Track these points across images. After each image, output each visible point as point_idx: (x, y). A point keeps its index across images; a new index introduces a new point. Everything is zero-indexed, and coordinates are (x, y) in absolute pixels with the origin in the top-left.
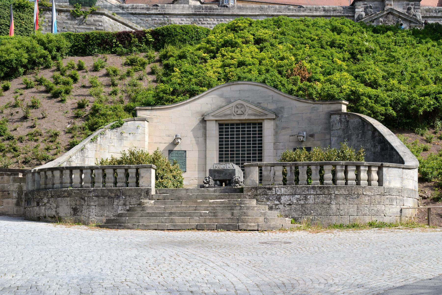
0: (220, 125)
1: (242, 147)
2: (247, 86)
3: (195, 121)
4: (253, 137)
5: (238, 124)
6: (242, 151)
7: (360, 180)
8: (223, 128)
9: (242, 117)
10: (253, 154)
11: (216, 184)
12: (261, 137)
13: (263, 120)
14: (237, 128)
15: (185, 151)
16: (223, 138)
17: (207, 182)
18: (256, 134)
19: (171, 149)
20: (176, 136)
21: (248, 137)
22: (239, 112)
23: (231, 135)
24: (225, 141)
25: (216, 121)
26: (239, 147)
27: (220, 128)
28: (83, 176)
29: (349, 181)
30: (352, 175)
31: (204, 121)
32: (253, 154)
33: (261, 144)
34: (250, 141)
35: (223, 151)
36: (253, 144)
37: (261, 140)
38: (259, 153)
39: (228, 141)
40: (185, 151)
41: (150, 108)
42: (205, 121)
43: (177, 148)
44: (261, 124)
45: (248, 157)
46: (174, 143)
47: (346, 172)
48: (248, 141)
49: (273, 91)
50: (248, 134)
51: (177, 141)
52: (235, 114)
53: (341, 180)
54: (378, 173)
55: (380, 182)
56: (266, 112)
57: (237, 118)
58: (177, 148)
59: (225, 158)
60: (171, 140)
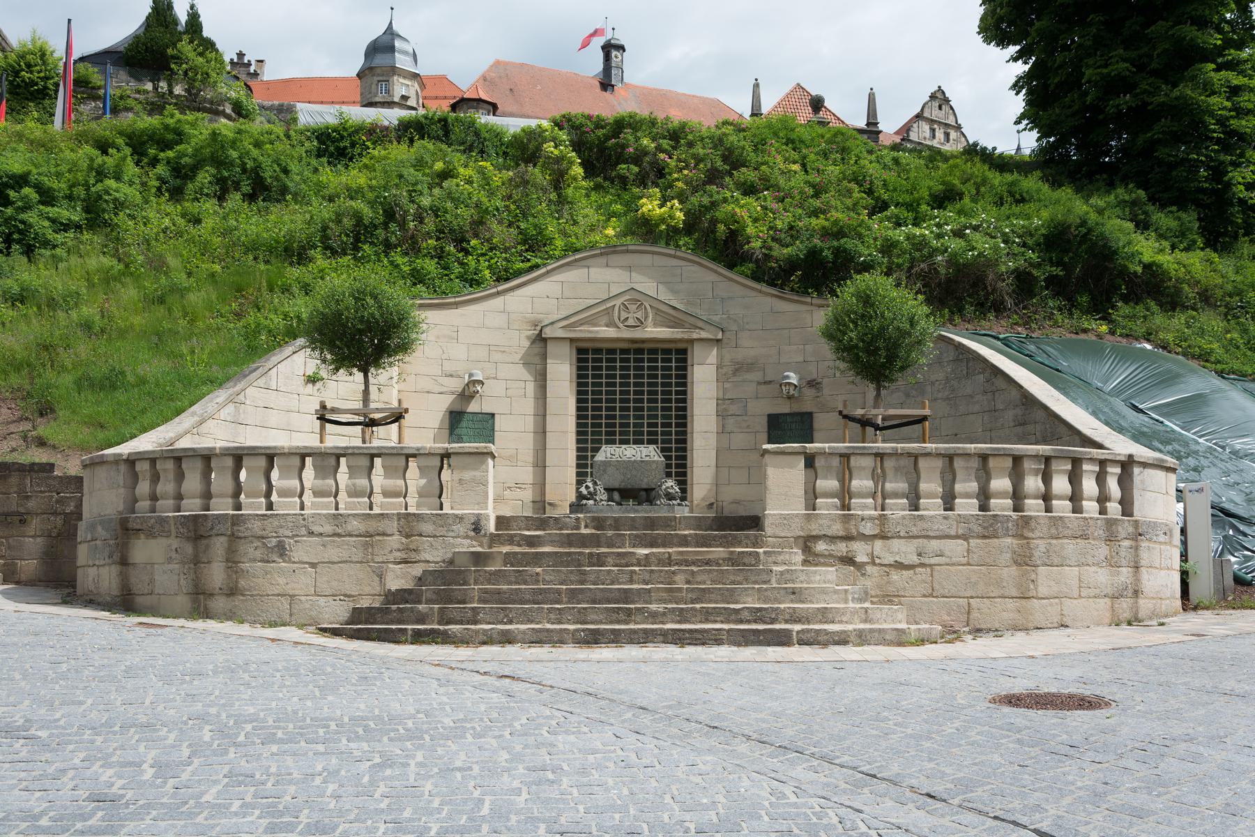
0: (580, 351)
1: (636, 409)
2: (649, 257)
3: (520, 341)
4: (663, 385)
5: (623, 351)
6: (636, 417)
7: (1082, 499)
8: (586, 360)
9: (637, 334)
10: (663, 425)
11: (610, 499)
12: (685, 385)
13: (692, 341)
14: (622, 360)
15: (493, 415)
16: (586, 384)
17: (590, 493)
18: (670, 376)
19: (457, 408)
20: (471, 375)
21: (608, 384)
22: (631, 322)
23: (608, 376)
24: (593, 393)
25: (572, 340)
26: (628, 409)
27: (579, 360)
28: (243, 475)
29: (1054, 502)
30: (1061, 484)
31: (541, 340)
32: (663, 425)
33: (684, 401)
34: (656, 393)
35: (586, 417)
36: (663, 401)
37: (685, 393)
38: (677, 425)
39: (600, 393)
40: (493, 415)
41: (796, 298)
42: (545, 340)
43: (473, 407)
44: (685, 351)
45: (649, 433)
46: (466, 395)
47: (1047, 479)
48: (649, 393)
49: (716, 272)
50: (649, 376)
51: (472, 389)
52: (621, 325)
53: (1036, 498)
54: (1120, 482)
55: (1127, 505)
56: (700, 324)
57: (610, 333)
58: (473, 407)
59: (593, 433)
60: (457, 385)
